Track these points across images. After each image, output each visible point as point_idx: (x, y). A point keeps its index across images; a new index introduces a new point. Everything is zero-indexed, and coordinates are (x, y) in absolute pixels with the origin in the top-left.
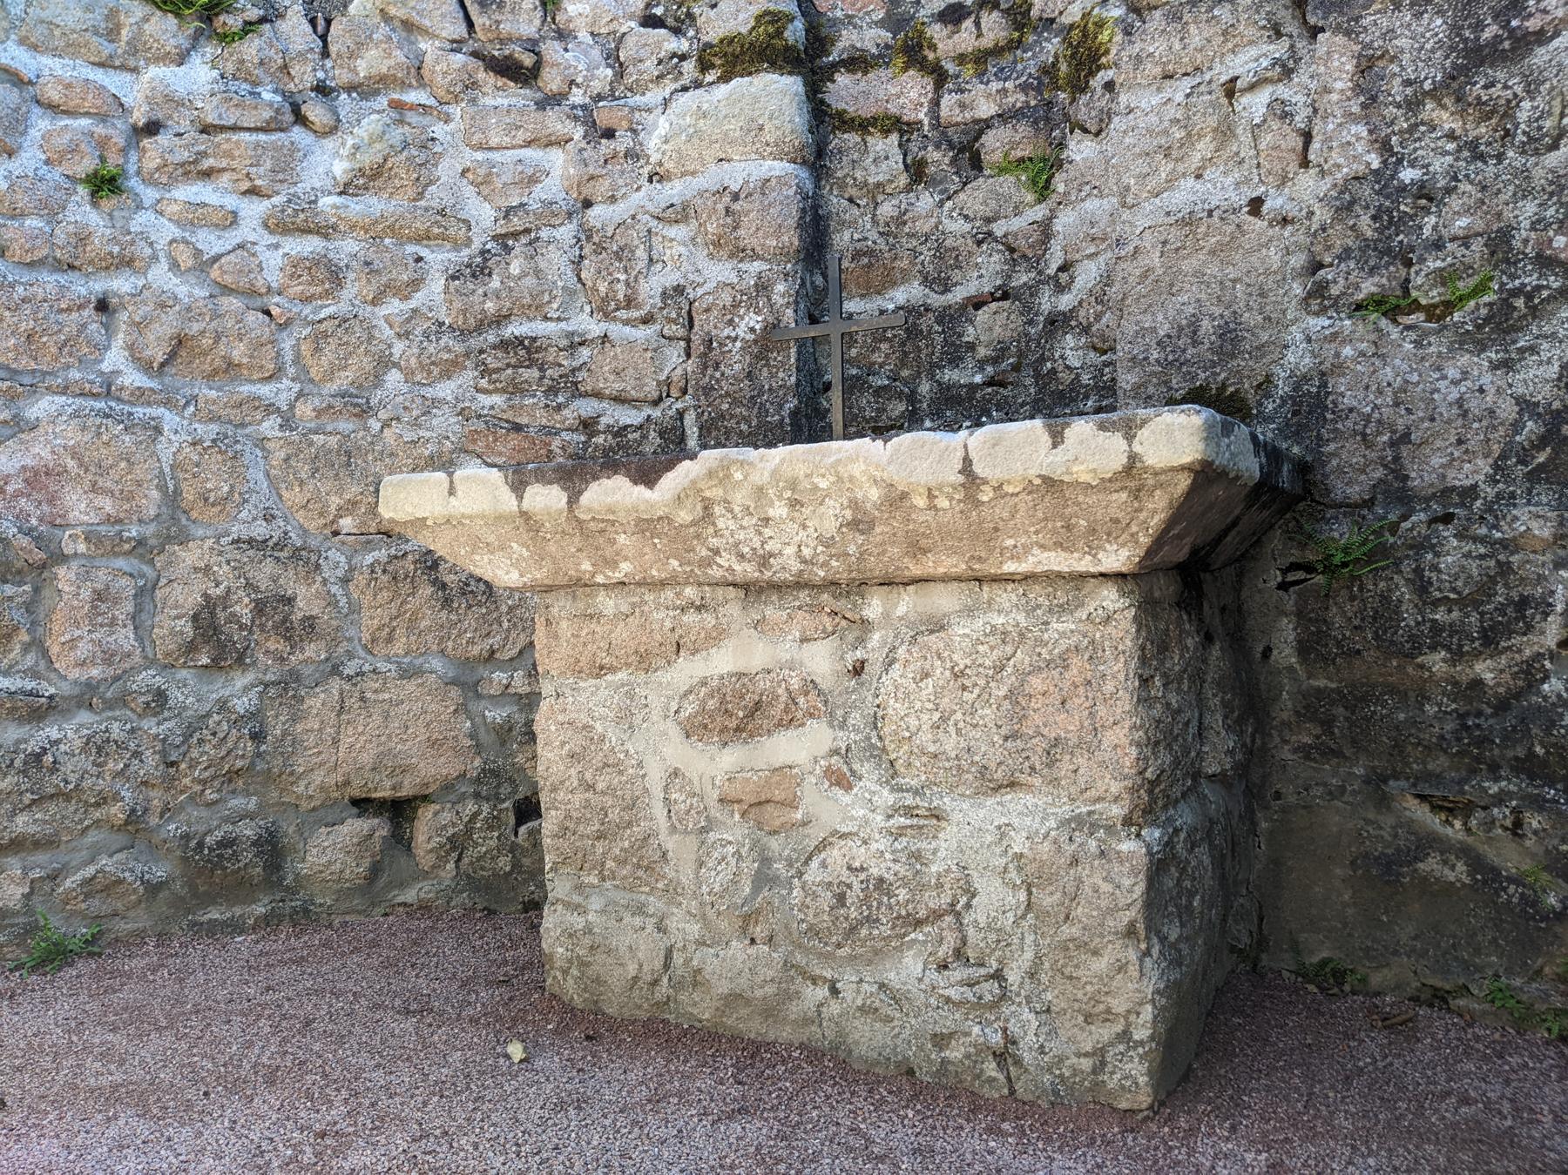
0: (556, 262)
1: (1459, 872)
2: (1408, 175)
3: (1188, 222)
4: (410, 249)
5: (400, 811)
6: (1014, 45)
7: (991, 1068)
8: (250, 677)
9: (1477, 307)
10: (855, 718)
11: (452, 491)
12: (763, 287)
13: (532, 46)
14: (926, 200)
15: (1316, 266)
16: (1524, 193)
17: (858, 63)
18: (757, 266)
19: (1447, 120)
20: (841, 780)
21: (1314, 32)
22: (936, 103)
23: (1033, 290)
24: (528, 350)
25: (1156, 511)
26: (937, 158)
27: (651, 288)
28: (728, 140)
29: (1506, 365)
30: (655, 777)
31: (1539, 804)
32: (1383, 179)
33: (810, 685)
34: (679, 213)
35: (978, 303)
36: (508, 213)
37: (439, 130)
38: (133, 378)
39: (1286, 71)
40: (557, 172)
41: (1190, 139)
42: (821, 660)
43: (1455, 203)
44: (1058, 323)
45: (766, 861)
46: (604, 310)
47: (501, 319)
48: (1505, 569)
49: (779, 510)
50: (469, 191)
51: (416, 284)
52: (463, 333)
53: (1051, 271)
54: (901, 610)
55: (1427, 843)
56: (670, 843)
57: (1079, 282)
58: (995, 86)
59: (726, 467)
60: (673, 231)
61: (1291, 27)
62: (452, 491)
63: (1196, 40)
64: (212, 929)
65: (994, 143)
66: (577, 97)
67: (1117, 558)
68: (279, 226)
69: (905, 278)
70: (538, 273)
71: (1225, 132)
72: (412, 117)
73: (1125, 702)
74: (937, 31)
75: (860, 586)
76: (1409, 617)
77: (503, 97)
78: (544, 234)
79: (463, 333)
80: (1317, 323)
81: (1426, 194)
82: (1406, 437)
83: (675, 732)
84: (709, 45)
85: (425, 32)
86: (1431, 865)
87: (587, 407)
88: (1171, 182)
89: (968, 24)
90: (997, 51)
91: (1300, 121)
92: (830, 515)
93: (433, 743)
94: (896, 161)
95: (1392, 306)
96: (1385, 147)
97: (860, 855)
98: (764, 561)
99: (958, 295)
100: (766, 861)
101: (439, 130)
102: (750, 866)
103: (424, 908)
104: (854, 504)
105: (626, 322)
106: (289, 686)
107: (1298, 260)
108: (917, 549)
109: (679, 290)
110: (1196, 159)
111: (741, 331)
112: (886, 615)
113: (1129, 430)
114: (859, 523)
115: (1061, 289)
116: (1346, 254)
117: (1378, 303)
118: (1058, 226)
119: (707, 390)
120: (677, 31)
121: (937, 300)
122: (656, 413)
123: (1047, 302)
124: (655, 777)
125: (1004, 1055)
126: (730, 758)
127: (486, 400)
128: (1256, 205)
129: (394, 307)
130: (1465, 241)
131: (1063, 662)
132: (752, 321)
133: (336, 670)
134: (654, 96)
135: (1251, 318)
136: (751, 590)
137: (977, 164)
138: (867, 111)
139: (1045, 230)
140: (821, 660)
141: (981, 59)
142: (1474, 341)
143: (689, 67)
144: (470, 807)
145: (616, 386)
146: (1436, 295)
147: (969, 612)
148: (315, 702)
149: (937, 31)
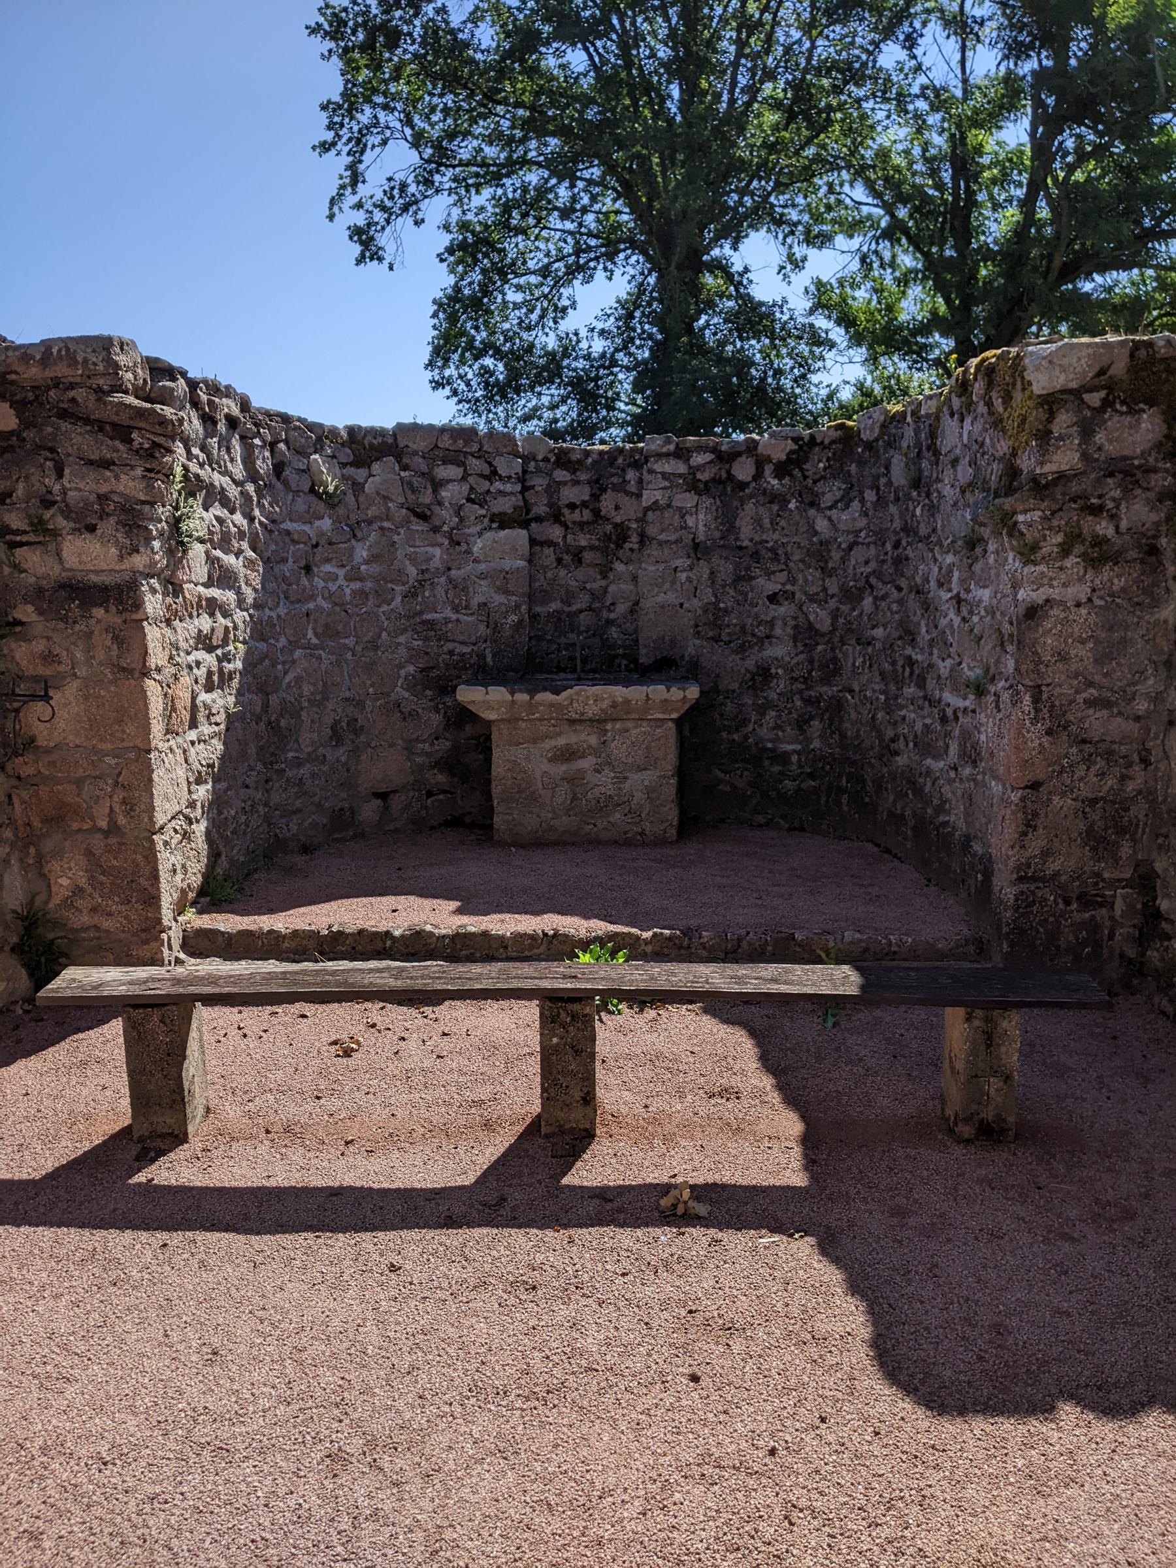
0: (440, 592)
1: (728, 788)
2: (722, 605)
3: (663, 607)
4: (390, 585)
5: (383, 796)
6: (593, 523)
7: (639, 837)
8: (345, 748)
9: (464, 171)
10: (603, 755)
11: (487, 693)
12: (518, 606)
13: (428, 507)
14: (562, 573)
15: (697, 626)
16: (748, 617)
17: (539, 519)
18: (514, 598)
19: (732, 593)
20: (598, 771)
21: (699, 559)
22: (565, 537)
23: (600, 609)
24: (430, 625)
25: (687, 706)
26: (567, 558)
27: (475, 602)
28: (504, 552)
29: (743, 659)
30: (538, 774)
31: (747, 769)
32: (715, 604)
33: (590, 747)
34: (482, 576)
35: (581, 611)
36: (423, 572)
37: (396, 538)
38: (315, 641)
39: (691, 568)
40: (438, 556)
41: (663, 583)
42: (593, 740)
43: (733, 615)
44: (609, 622)
45: (575, 794)
46: (456, 609)
47: (421, 613)
48: (741, 711)
49: (591, 702)
50: (407, 562)
51: (393, 599)
52: (408, 618)
53: (608, 604)
54: (617, 726)
55: (720, 781)
56: (542, 792)
57: (618, 610)
58: (588, 536)
59: (581, 690)
60: (482, 582)
61: (692, 555)
62: (487, 693)
63: (666, 552)
64: (337, 840)
65: (587, 556)
66: (445, 528)
67: (675, 716)
68: (348, 579)
69: (555, 599)
70: (435, 596)
71: (673, 582)
72: (387, 534)
73: (673, 748)
74: (566, 511)
75: (605, 721)
76: (718, 723)
77: (418, 526)
78: (436, 580)
79: (408, 618)
80: (697, 642)
81: (726, 611)
82: (718, 676)
83: (545, 761)
84: (494, 514)
85: (391, 500)
86: (721, 787)
87: (450, 645)
88: (657, 595)
89: (578, 511)
90: (588, 523)
91: (694, 584)
92: (605, 704)
93: (400, 771)
94: (553, 557)
95: (716, 640)
96: (716, 597)
97: (603, 790)
98: (582, 714)
99: (574, 608)
100: (575, 794)
101: (396, 538)
102: (569, 797)
103: (397, 831)
104: (614, 702)
105: (467, 615)
106: (355, 752)
107: (692, 623)
108: (628, 713)
109: (485, 604)
110: (665, 588)
111: (509, 621)
112: (613, 728)
113: (684, 690)
114: (614, 705)
115: (610, 611)
116: (705, 624)
117: (712, 638)
118: (610, 589)
119: (495, 641)
120: (481, 506)
121: (567, 609)
122: (475, 648)
123: (605, 614)
124: (538, 774)
125: (642, 834)
126: (564, 767)
127: (416, 643)
128: (681, 605)
129: (385, 608)
130: (735, 626)
131: (659, 739)
132: (513, 618)
133: (369, 745)
134: (474, 530)
135: (679, 638)
136: (572, 722)
137: (580, 561)
138: (543, 539)
139: (605, 590)
140: (593, 740)
141: (581, 525)
142: (736, 652)
143: (486, 520)
144: (411, 794)
145: (461, 638)
146: (727, 639)
147: (636, 727)
148: (363, 757)
149: (566, 511)
